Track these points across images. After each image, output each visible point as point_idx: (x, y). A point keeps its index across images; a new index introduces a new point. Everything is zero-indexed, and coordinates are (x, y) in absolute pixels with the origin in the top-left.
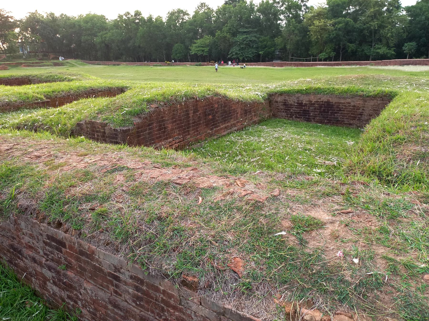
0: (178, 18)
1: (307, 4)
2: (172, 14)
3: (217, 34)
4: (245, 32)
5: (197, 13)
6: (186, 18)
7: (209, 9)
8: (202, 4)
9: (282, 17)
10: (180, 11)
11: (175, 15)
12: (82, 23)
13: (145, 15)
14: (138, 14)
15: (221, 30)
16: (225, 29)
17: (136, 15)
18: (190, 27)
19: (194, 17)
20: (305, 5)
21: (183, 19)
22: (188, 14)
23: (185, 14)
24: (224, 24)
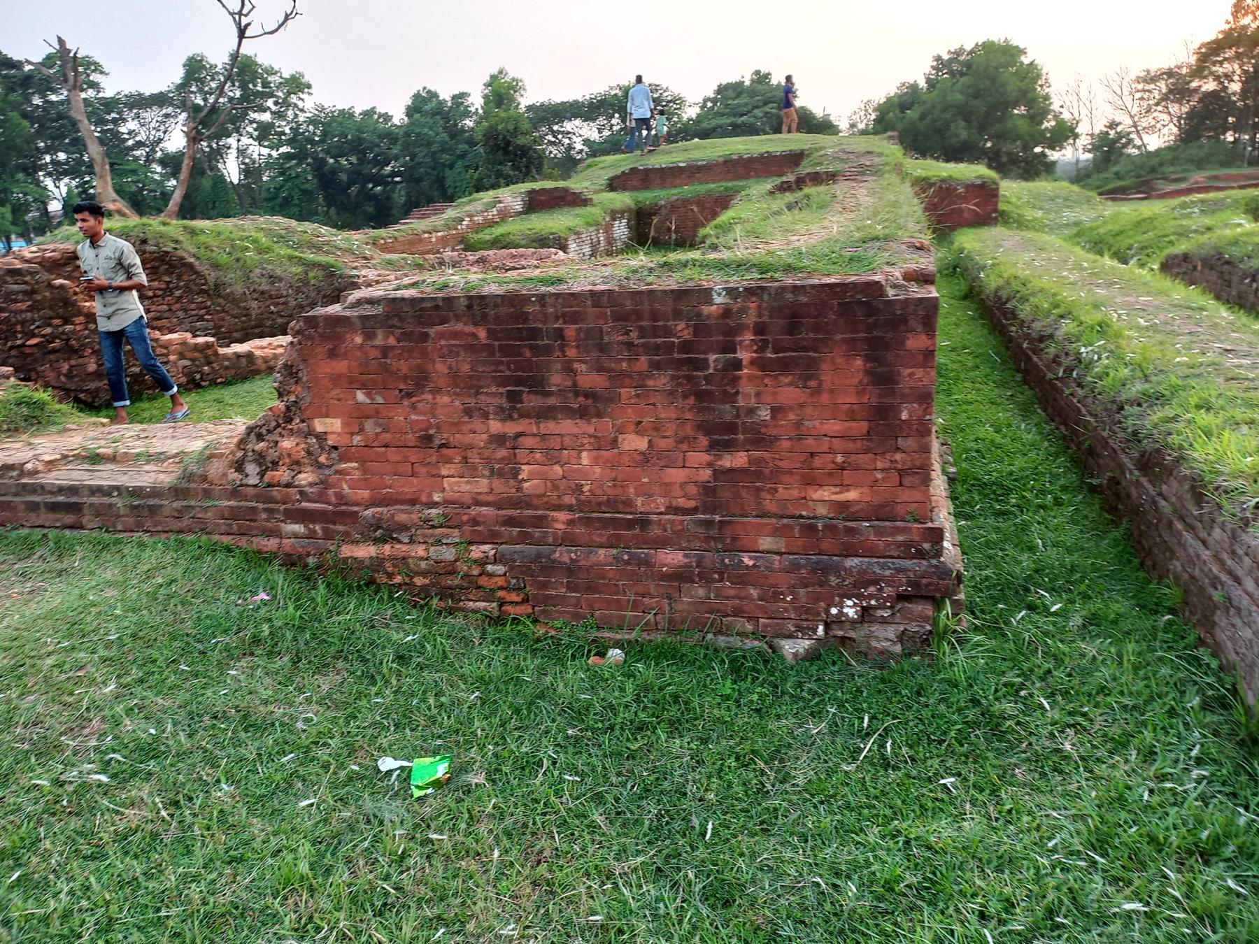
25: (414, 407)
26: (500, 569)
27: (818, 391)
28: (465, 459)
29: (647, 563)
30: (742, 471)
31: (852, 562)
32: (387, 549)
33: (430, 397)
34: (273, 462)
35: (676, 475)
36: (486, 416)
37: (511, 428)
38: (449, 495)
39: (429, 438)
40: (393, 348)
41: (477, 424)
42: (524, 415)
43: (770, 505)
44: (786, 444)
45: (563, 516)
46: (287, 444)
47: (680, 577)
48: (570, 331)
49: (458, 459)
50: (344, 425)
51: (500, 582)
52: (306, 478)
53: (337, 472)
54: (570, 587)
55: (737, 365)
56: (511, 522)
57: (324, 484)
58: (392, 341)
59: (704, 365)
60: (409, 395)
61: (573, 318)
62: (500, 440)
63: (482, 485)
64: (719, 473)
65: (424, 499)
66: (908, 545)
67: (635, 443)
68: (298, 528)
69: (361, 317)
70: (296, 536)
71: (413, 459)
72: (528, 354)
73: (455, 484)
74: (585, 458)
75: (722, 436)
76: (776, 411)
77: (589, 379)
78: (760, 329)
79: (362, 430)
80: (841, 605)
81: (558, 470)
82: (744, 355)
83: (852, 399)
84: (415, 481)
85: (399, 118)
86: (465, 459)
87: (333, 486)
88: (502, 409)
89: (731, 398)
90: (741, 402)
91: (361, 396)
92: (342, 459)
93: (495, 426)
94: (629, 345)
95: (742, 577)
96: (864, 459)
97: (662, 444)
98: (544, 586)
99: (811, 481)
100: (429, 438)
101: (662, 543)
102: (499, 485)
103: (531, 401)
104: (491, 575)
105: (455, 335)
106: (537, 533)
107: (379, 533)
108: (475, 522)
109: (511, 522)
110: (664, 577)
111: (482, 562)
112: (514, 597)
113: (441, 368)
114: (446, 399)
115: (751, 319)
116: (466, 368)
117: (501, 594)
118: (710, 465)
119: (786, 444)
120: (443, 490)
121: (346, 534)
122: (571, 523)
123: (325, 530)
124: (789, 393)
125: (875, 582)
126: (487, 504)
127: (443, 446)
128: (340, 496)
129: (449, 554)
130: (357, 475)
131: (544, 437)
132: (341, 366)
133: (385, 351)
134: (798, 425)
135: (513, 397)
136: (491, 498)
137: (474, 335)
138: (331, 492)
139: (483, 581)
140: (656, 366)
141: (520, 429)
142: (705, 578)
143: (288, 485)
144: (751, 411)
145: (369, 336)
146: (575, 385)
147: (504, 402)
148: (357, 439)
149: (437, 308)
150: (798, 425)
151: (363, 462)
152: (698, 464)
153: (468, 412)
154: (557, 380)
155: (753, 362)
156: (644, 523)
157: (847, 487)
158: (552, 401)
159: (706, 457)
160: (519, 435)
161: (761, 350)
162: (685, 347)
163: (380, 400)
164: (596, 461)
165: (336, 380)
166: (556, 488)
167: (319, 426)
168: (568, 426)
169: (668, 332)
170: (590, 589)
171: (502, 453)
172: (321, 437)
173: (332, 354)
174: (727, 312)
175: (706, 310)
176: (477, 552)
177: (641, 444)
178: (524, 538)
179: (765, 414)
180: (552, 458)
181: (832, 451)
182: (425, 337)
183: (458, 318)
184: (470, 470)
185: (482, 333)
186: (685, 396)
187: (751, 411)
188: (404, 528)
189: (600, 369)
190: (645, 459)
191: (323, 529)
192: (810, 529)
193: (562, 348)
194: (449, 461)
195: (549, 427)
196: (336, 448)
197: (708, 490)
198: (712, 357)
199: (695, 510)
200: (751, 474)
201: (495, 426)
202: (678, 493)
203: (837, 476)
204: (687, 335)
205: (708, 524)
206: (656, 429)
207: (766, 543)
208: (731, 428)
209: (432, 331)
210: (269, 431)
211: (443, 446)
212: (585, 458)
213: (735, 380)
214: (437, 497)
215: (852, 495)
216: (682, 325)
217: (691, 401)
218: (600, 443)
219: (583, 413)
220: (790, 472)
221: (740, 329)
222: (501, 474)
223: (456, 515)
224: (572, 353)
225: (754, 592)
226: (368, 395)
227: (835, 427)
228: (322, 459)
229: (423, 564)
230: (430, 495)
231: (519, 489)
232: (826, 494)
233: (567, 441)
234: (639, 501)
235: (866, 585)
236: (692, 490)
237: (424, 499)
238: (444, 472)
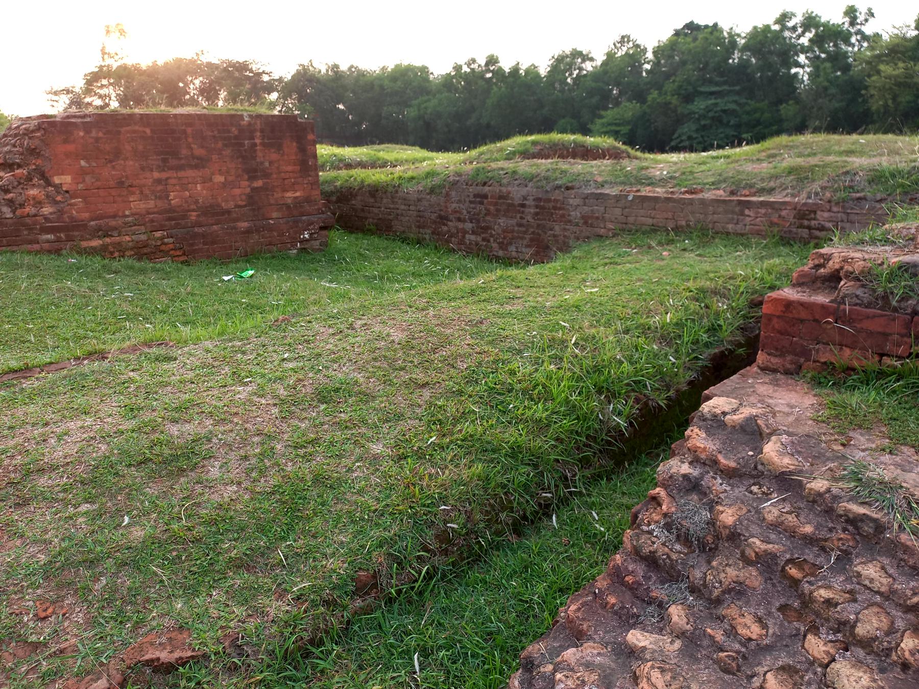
0: (570, 67)
1: (863, 28)
2: (560, 60)
3: (650, 98)
4: (712, 93)
5: (610, 56)
6: (588, 66)
7: (638, 46)
8: (623, 37)
9: (802, 59)
10: (576, 54)
11: (564, 63)
12: (386, 82)
13: (506, 65)
14: (492, 61)
15: (660, 88)
16: (669, 86)
17: (487, 64)
18: (593, 85)
19: (604, 64)
20: (859, 32)
21: (581, 69)
22: (592, 59)
23: (586, 58)
24: (667, 76)
25: (113, 167)
26: (171, 240)
27: (283, 155)
28: (141, 193)
29: (235, 228)
30: (261, 188)
31: (304, 218)
32: (108, 240)
33: (122, 162)
34: (20, 205)
35: (237, 191)
36: (152, 171)
37: (164, 175)
38: (134, 211)
39: (123, 183)
40: (101, 138)
41: (148, 174)
42: (171, 168)
43: (272, 202)
44: (275, 176)
45: (194, 214)
46: (33, 192)
47: (248, 232)
48: (189, 130)
49: (138, 192)
50: (73, 179)
51: (171, 246)
52: (47, 210)
53: (69, 205)
54: (205, 244)
55: (255, 145)
56: (170, 219)
57: (61, 212)
58: (101, 134)
59: (243, 145)
60: (111, 161)
61: (190, 125)
62: (159, 181)
63: (151, 204)
64: (253, 189)
65: (120, 214)
66: (319, 209)
67: (219, 179)
68: (50, 237)
69: (82, 123)
70: (48, 241)
71: (113, 194)
72: (170, 140)
73: (137, 205)
74: (199, 187)
75: (252, 174)
76: (271, 163)
77: (199, 152)
78: (262, 131)
79: (84, 181)
80: (304, 234)
81: (187, 193)
82: (258, 141)
83: (294, 157)
84: (115, 205)
85: (507, 70)
86: (141, 193)
87: (66, 212)
88: (159, 167)
89: (254, 158)
90: (258, 160)
91: (83, 163)
92: (72, 198)
93: (156, 175)
94: (214, 137)
95: (271, 229)
96: (300, 180)
97: (230, 179)
98: (192, 245)
99: (285, 190)
100: (123, 183)
101: (237, 220)
102: (160, 203)
103: (173, 162)
104: (166, 244)
105: (135, 132)
106: (183, 222)
107: (100, 233)
108: (152, 221)
109: (170, 219)
110: (244, 233)
111: (162, 238)
112: (178, 253)
113: (128, 147)
114: (131, 163)
115: (258, 126)
116: (141, 147)
117: (171, 252)
118: (249, 186)
119: (275, 176)
120: (131, 209)
121: (82, 236)
122: (198, 216)
123: (66, 236)
124: (274, 156)
125: (312, 224)
126: (154, 213)
127: (130, 186)
128: (72, 218)
129: (143, 237)
130: (81, 205)
131: (179, 179)
132: (71, 147)
133: (97, 140)
134: (278, 168)
135: (165, 161)
136: (156, 210)
137: (145, 132)
138: (65, 216)
139: (163, 247)
140: (225, 145)
141: (168, 175)
142: (258, 231)
143: (35, 215)
144: (262, 163)
145: (88, 132)
146: (192, 154)
147: (161, 163)
148: (80, 186)
149: (124, 119)
150: (278, 168)
151: (85, 199)
152: (244, 188)
153: (142, 169)
154: (184, 152)
155: (261, 144)
156: (229, 212)
157: (296, 191)
158: (183, 162)
159: (247, 183)
160: (167, 179)
161: (263, 139)
162: (236, 137)
163: (95, 164)
164: (203, 188)
165: (68, 155)
166: (186, 202)
167: (57, 180)
168: (190, 173)
169: (229, 132)
170: (213, 243)
171: (160, 188)
172: (58, 187)
173: (66, 141)
174: (250, 124)
175: (242, 123)
176: (158, 234)
177: (221, 179)
178: (177, 226)
179: (267, 164)
180: (184, 187)
181: (290, 178)
182: (119, 133)
183: (135, 124)
184: (144, 197)
185: (148, 131)
186: (237, 158)
187: (262, 163)
188: (115, 229)
189: (202, 147)
190: (224, 185)
191: (66, 236)
192: (288, 207)
193: (186, 138)
194: (134, 193)
195: (181, 174)
196: (67, 192)
197: (250, 197)
198: (246, 142)
199: (245, 206)
200: (264, 188)
201: (156, 175)
202: (238, 199)
203: (292, 187)
204: (236, 133)
205: (254, 210)
206: (227, 172)
207: (275, 215)
208: (256, 171)
209: (123, 130)
210: (13, 188)
211: (130, 186)
212: (199, 187)
213: (255, 151)
214: (127, 213)
215: (298, 194)
216: (234, 129)
217: (240, 160)
218: (206, 180)
219: (196, 167)
220: (277, 186)
221: (255, 130)
222: (160, 198)
223: (140, 219)
224: (190, 140)
225: (275, 234)
226: (87, 162)
227: (290, 168)
228: (59, 198)
229: (130, 244)
230: (124, 212)
231: (170, 204)
232: (289, 194)
233: (190, 180)
234: (223, 204)
235: (310, 225)
236: (244, 197)
237: (120, 214)
238: (131, 199)
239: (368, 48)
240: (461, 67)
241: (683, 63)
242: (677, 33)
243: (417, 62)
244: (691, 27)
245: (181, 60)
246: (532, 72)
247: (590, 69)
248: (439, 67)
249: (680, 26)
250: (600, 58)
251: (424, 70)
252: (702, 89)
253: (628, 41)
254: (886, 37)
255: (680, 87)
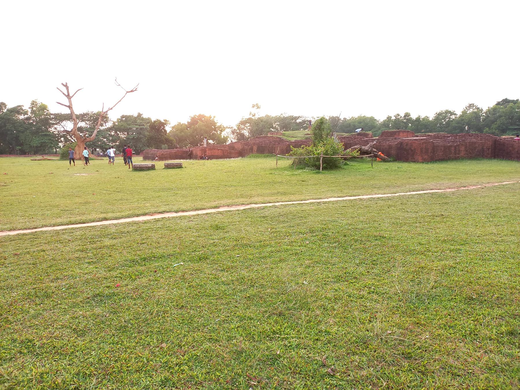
2: (440, 114)
4: (515, 129)
5: (464, 112)
6: (453, 117)
7: (478, 108)
8: (470, 105)
10: (447, 112)
13: (414, 117)
17: (405, 116)
18: (456, 125)
22: (455, 114)
23: (452, 113)
24: (493, 122)
239: (348, 110)
240: (391, 117)
241: (500, 116)
242: (498, 104)
243: (368, 115)
244: (506, 101)
245: (203, 116)
246: (426, 119)
247: (454, 118)
248: (381, 117)
249: (500, 100)
250: (459, 113)
251: (372, 119)
252: (511, 127)
253: (473, 107)
254: (313, 121)
255: (499, 126)
